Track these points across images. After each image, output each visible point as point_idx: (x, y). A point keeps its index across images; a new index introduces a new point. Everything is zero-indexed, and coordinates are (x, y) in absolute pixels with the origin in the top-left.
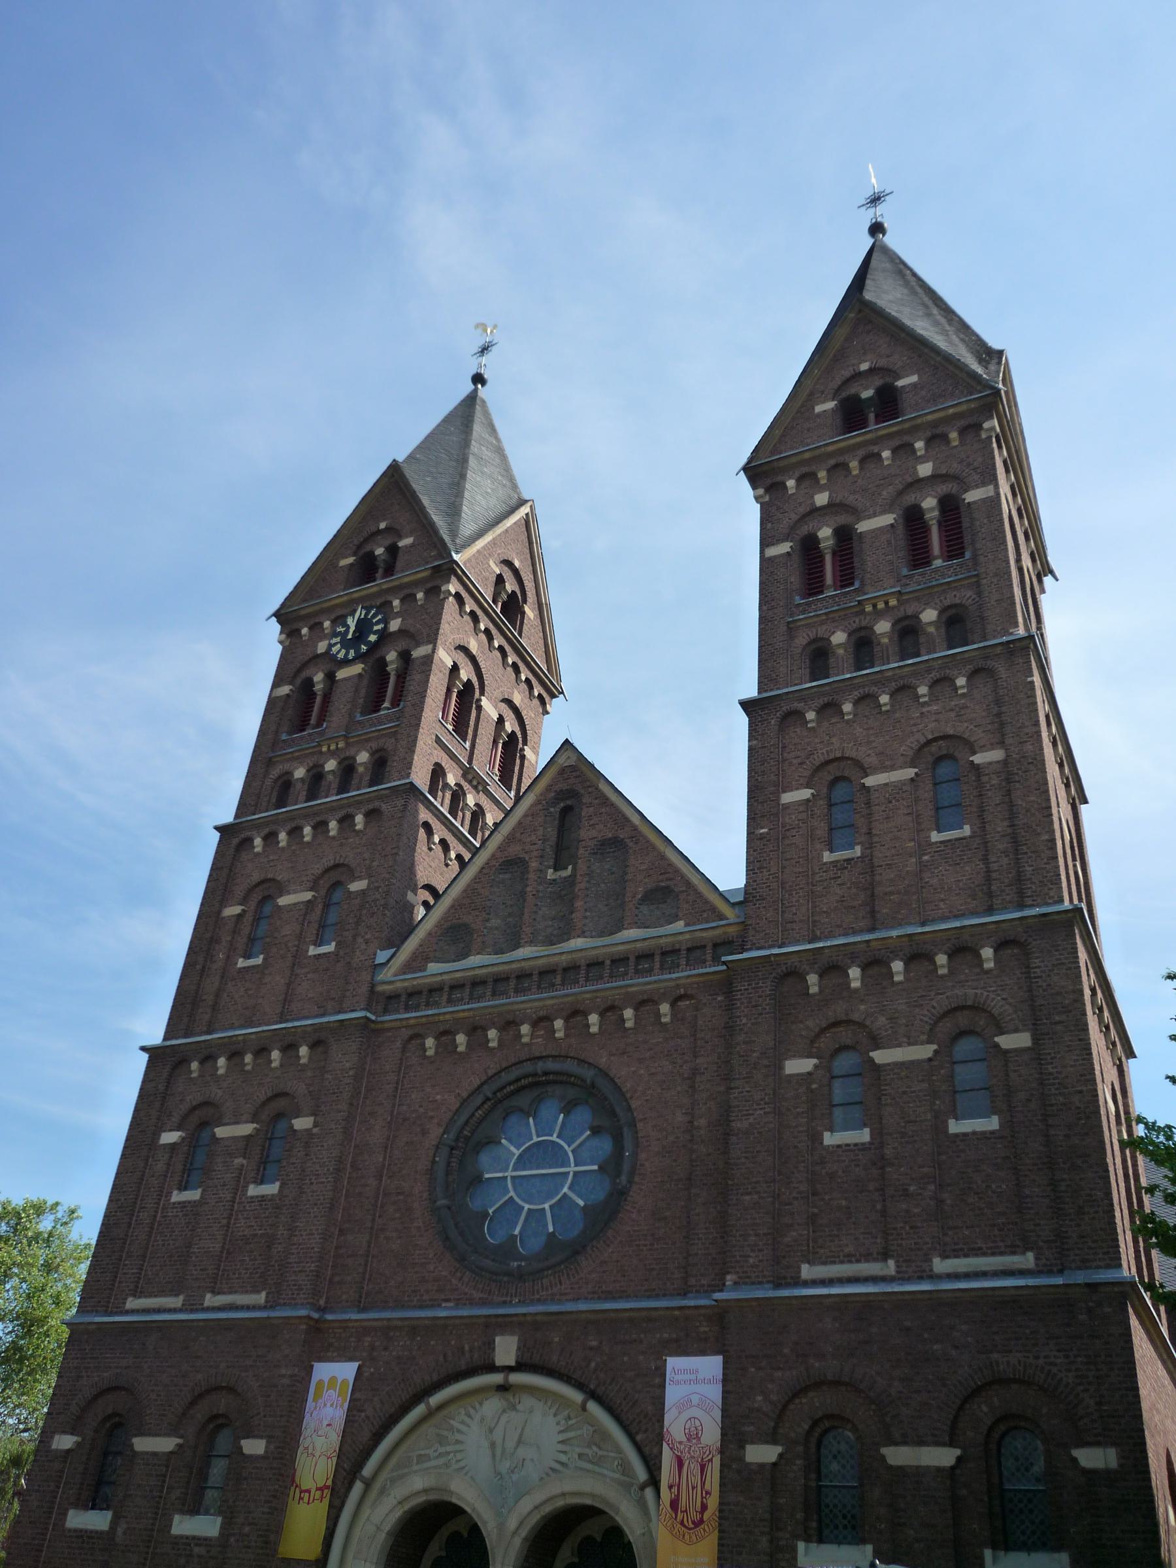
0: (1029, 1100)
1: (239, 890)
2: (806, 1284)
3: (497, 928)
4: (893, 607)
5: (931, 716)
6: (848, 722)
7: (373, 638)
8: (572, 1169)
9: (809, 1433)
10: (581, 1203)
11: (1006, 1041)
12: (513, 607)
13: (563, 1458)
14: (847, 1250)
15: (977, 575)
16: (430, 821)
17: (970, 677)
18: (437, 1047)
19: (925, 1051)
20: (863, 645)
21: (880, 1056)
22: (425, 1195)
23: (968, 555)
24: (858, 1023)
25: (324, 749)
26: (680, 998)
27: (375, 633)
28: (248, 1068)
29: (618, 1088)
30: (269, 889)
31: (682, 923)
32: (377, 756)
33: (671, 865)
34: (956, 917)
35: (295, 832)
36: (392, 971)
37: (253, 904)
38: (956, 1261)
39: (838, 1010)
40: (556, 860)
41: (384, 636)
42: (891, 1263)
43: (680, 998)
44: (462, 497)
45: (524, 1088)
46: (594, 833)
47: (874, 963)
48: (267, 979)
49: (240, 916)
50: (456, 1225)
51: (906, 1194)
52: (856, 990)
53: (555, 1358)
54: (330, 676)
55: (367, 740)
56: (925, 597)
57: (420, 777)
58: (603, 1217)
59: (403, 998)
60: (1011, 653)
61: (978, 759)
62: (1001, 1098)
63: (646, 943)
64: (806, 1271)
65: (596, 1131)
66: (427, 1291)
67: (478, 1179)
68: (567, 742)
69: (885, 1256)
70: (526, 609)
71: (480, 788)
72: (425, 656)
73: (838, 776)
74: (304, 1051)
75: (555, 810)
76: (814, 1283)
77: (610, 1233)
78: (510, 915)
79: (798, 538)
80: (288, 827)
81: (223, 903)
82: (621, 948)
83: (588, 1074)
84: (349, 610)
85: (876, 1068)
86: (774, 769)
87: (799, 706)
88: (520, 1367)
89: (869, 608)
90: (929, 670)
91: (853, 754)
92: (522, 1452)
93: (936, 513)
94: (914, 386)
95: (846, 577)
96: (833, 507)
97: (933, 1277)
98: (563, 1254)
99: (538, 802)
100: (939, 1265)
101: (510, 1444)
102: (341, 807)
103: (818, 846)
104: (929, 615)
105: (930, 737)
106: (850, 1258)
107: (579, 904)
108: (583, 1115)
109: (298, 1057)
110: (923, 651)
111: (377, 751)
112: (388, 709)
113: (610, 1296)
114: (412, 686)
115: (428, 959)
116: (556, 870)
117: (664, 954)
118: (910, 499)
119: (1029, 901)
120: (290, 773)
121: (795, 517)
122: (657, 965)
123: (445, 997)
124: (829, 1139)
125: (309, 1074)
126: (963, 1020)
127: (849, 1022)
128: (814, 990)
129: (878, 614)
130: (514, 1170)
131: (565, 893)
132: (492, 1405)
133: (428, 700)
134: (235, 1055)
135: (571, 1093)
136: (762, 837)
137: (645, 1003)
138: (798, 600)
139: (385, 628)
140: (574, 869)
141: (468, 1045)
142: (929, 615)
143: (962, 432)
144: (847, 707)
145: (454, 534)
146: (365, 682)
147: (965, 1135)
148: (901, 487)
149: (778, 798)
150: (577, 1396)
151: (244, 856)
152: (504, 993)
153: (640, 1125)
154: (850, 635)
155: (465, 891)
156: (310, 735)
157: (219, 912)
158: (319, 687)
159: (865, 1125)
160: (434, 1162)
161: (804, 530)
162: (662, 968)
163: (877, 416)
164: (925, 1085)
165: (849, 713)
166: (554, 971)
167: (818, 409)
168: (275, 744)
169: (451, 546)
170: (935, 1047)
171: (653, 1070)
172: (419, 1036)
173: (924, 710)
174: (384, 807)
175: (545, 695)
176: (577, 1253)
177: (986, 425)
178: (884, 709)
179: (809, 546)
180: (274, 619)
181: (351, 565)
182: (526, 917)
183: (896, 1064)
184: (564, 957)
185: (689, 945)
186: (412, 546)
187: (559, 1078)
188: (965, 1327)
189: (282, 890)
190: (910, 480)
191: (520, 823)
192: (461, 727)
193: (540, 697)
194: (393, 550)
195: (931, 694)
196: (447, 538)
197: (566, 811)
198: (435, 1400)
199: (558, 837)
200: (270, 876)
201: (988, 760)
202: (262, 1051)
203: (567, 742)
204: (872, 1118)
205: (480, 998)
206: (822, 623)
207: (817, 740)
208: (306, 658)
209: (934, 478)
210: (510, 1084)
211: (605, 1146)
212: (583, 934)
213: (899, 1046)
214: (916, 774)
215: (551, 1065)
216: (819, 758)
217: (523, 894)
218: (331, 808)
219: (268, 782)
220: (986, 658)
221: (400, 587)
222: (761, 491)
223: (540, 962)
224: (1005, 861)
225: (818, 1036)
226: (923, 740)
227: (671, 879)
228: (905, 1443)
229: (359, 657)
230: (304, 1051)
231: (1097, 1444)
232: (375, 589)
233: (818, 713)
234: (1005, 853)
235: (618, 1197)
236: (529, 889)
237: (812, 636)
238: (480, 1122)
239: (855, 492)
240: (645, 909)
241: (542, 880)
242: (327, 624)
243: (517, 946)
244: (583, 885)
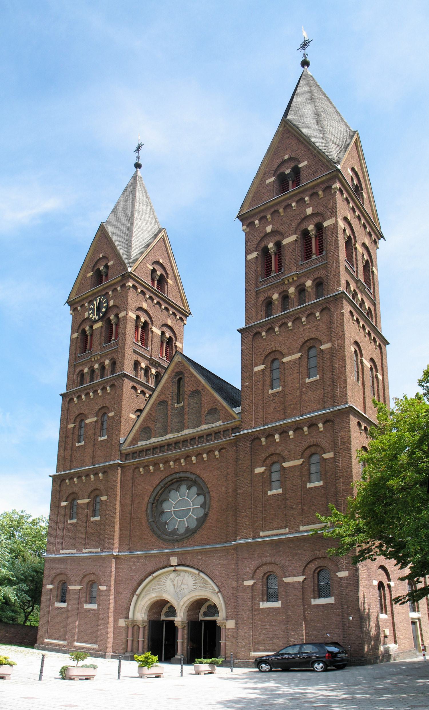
0: (331, 475)
1: (72, 418)
3: (159, 427)
4: (296, 281)
5: (307, 330)
6: (277, 335)
7: (104, 310)
8: (192, 507)
9: (263, 576)
10: (196, 517)
11: (325, 456)
12: (162, 281)
13: (195, 587)
14: (275, 526)
15: (326, 263)
16: (135, 385)
17: (321, 312)
18: (144, 471)
19: (299, 462)
20: (285, 297)
21: (285, 465)
22: (146, 518)
23: (324, 252)
24: (278, 454)
25: (93, 360)
26: (222, 449)
27: (104, 307)
28: (84, 481)
29: (203, 481)
30: (81, 417)
31: (221, 421)
32: (112, 361)
33: (216, 399)
35: (87, 394)
36: (126, 445)
37: (78, 423)
38: (307, 526)
39: (272, 450)
40: (178, 400)
41: (108, 308)
42: (287, 529)
43: (222, 449)
44: (132, 236)
45: (174, 482)
46: (189, 388)
47: (283, 432)
48: (86, 450)
49: (74, 428)
50: (157, 527)
51: (292, 508)
52: (278, 442)
53: (189, 562)
54: (91, 327)
55: (108, 355)
56: (306, 275)
57: (128, 370)
58: (202, 521)
59: (131, 455)
60: (336, 300)
61: (322, 347)
62: (323, 475)
63: (209, 430)
64: (262, 534)
65: (198, 495)
66: (149, 546)
67: (163, 512)
69: (286, 527)
70: (169, 280)
71: (157, 365)
72: (124, 317)
73: (273, 358)
74: (100, 475)
75: (176, 380)
76: (264, 537)
77: (203, 526)
78: (163, 422)
79: (260, 249)
80: (85, 393)
81: (67, 423)
82: (200, 432)
83: (193, 477)
84: (94, 297)
85: (284, 468)
86: (251, 358)
87: (259, 330)
88: (178, 565)
89: (286, 282)
90: (306, 310)
92: (182, 586)
93: (314, 232)
94: (306, 166)
95: (279, 267)
96: (274, 232)
97: (300, 532)
98: (190, 533)
99: (169, 377)
100: (302, 528)
101: (179, 585)
102: (101, 384)
103: (267, 388)
104: (309, 283)
105: (306, 339)
106: (276, 529)
107: (186, 417)
108: (194, 490)
109: (99, 477)
110: (307, 300)
111: (112, 359)
112: (114, 340)
113: (204, 544)
114: (121, 331)
115: (138, 440)
116: (178, 403)
117: (216, 433)
118: (303, 226)
119: (336, 404)
120: (83, 370)
121: (259, 239)
122: (213, 438)
123: (144, 454)
124: (270, 493)
125: (104, 482)
126: (313, 450)
127: (276, 454)
128: (264, 443)
129: (290, 284)
130: (174, 508)
131: (181, 412)
132: (173, 575)
133: (127, 336)
134: (79, 477)
135: (190, 483)
136: (246, 386)
137: (210, 452)
138: (260, 279)
139: (108, 304)
140: (184, 403)
141: (154, 470)
142: (309, 283)
143: (324, 190)
144: (277, 329)
145: (129, 257)
146: (104, 329)
147: (312, 488)
148: (300, 220)
149: (253, 370)
150: (196, 572)
151: (72, 405)
152: (164, 451)
153: (211, 493)
154: (279, 294)
155: (147, 414)
156: (87, 353)
157: (67, 427)
158: (88, 332)
159: (281, 488)
160: (147, 508)
161: (263, 245)
162: (215, 439)
163: (293, 182)
164: (299, 473)
165: (277, 332)
166: (179, 442)
167: (268, 181)
168: (76, 358)
169: (127, 265)
170: (303, 460)
171: (214, 474)
172: (138, 468)
173: (305, 327)
174: (116, 383)
175: (183, 317)
176: (193, 533)
177: (333, 187)
178: (290, 328)
179: (265, 251)
180: (67, 304)
181: (92, 276)
182: (168, 423)
184: (182, 437)
185: (224, 430)
186: (113, 265)
187: (185, 479)
188: (307, 545)
189: (87, 418)
190: (303, 217)
191: (164, 386)
192: (145, 341)
193: (180, 318)
194: (106, 266)
195: (307, 320)
196: (126, 260)
197: (180, 379)
198: (155, 575)
199: (178, 391)
200: (81, 412)
201: (326, 348)
202: (87, 476)
204: (282, 485)
205: (156, 453)
206: (269, 290)
207: (266, 344)
208: (81, 320)
209: (313, 215)
210: (169, 481)
211: (201, 499)
212: (188, 428)
213: (292, 460)
214: (301, 355)
215: (181, 475)
216: (267, 352)
217: (167, 414)
218: (98, 385)
219: (76, 375)
220: (327, 303)
221: (111, 285)
222: (245, 227)
223: (174, 439)
224: (330, 389)
225: (266, 459)
226: (304, 341)
227: (216, 405)
229: (101, 319)
230: (100, 475)
232: (101, 288)
233: (266, 332)
234: (330, 386)
235: (206, 515)
236: (169, 412)
237: (266, 296)
238: (161, 494)
239: (282, 225)
240: (209, 417)
241: (173, 408)
242: (86, 304)
243: (166, 434)
244: (187, 410)
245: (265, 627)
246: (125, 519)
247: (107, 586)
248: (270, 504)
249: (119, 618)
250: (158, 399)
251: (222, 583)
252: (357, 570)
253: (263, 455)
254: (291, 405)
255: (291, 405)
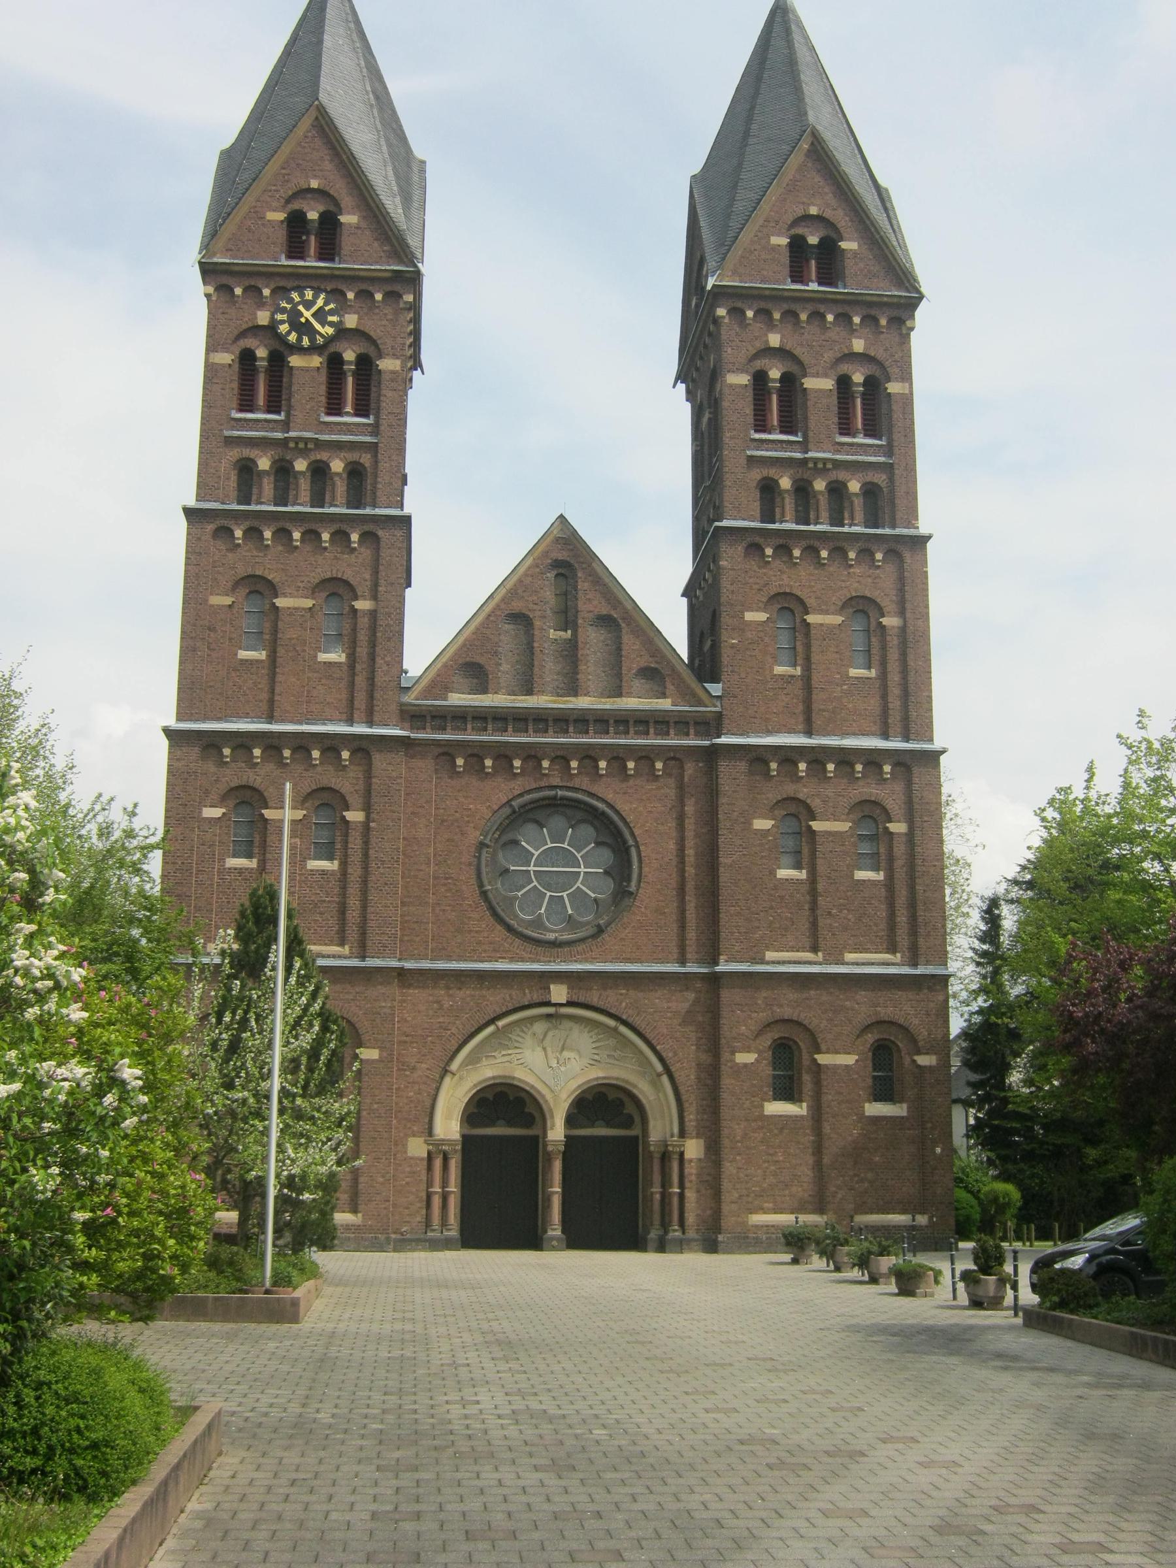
2: (768, 963)
8: (582, 869)
13: (596, 1057)
31: (669, 701)
34: (246, 420)
45: (543, 806)
53: (595, 1000)
66: (485, 951)
68: (561, 516)
88: (570, 1004)
91: (799, 593)
106: (792, 949)
183: (826, 832)
203: (561, 516)
228: (827, 1052)
231: (927, 1054)
245: (775, 1159)
246: (416, 877)
247: (381, 1048)
248: (782, 898)
249: (407, 1136)
250: (503, 606)
251: (675, 1054)
252: (718, 996)
253: (770, 796)
254: (824, 710)
255: (824, 710)
